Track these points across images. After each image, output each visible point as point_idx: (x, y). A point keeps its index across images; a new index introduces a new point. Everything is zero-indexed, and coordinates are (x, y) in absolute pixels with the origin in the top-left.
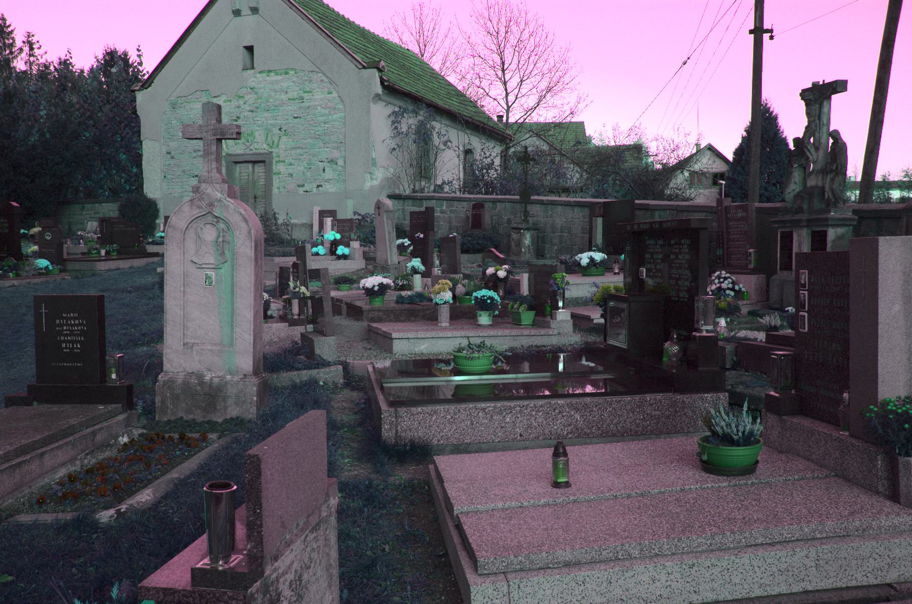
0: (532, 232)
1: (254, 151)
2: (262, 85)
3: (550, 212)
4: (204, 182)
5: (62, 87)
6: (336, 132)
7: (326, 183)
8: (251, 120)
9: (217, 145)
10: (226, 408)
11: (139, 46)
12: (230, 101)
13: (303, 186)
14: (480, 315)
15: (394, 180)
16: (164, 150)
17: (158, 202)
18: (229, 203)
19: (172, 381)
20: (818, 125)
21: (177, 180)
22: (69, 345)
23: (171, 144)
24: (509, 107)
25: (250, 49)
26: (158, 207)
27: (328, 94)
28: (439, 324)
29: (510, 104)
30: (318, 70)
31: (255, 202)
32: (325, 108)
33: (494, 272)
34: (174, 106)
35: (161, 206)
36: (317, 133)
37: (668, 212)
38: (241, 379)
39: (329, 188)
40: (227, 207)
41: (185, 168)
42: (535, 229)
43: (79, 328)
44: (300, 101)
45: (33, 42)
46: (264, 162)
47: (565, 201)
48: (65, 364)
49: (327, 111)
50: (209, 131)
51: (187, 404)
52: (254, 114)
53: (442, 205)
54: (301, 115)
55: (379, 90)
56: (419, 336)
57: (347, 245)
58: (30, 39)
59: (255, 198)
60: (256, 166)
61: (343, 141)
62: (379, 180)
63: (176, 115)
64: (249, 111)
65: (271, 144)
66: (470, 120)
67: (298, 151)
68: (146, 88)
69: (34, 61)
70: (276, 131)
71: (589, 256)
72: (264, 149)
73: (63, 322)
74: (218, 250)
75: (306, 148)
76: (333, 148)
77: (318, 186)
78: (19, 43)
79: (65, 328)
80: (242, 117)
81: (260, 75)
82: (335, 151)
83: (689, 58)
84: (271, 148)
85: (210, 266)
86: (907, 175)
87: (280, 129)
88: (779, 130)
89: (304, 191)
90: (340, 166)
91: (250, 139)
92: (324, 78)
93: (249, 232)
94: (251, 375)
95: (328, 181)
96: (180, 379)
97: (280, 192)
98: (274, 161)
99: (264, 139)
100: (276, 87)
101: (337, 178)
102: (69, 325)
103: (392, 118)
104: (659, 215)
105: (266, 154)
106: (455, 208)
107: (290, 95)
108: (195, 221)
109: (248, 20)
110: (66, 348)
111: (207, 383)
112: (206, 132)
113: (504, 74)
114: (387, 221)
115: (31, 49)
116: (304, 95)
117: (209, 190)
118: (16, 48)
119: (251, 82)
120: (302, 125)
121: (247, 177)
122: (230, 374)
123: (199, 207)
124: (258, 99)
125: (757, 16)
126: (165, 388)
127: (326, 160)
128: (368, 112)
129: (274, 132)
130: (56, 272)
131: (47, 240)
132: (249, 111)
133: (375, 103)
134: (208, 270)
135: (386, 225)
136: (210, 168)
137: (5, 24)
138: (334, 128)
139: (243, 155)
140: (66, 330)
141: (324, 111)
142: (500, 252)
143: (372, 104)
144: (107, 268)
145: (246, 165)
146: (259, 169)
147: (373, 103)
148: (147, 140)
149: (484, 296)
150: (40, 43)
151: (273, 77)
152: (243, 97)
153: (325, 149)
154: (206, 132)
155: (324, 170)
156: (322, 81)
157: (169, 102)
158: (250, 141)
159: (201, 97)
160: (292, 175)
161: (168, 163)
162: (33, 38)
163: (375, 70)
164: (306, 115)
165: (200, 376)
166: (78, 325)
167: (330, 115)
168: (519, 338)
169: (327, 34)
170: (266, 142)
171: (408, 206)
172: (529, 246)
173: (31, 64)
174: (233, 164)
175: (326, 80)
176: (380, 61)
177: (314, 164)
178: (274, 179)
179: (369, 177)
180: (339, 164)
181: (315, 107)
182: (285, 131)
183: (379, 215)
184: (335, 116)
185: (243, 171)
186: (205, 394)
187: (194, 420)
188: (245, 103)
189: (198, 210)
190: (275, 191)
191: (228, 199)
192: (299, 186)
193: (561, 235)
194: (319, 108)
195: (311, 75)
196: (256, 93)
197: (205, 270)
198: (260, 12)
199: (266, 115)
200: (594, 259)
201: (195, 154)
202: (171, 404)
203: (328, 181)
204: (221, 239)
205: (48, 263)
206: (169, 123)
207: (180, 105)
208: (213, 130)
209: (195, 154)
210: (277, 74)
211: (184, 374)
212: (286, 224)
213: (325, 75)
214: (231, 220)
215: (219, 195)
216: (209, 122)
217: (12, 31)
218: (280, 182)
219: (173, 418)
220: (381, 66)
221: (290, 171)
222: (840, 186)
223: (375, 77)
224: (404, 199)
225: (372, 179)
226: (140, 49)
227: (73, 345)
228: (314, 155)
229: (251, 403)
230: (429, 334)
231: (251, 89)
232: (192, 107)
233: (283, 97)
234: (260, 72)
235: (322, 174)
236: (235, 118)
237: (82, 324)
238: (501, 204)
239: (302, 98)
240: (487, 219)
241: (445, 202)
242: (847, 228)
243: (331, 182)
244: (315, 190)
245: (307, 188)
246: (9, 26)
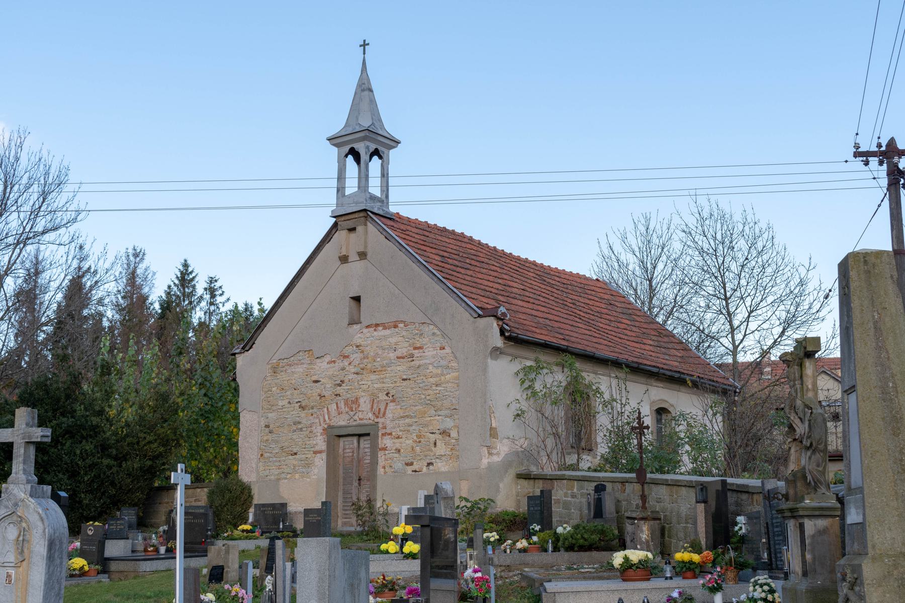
0: (652, 522)
1: (359, 422)
2: (369, 342)
3: (675, 496)
4: (12, 483)
5: (179, 350)
7: (438, 460)
8: (356, 384)
9: (25, 448)
11: (261, 299)
12: (334, 362)
13: (411, 464)
16: (263, 424)
17: (252, 487)
20: (799, 390)
21: (275, 459)
23: (270, 415)
25: (357, 299)
26: (252, 494)
30: (429, 322)
31: (360, 485)
32: (437, 367)
34: (275, 370)
35: (255, 491)
36: (428, 398)
39: (441, 466)
40: (27, 507)
41: (283, 445)
42: (654, 519)
44: (410, 359)
45: (215, 288)
46: (368, 435)
49: (439, 371)
50: (19, 435)
52: (359, 377)
53: (573, 487)
54: (410, 377)
55: (499, 342)
58: (213, 285)
59: (360, 480)
60: (362, 439)
62: (503, 455)
63: (276, 381)
64: (354, 373)
65: (377, 413)
67: (408, 421)
68: (248, 351)
69: (214, 311)
70: (382, 397)
72: (370, 419)
74: (18, 548)
75: (415, 416)
76: (446, 416)
77: (429, 464)
78: (200, 290)
80: (346, 379)
81: (367, 330)
82: (448, 419)
84: (377, 417)
85: (11, 565)
87: (387, 394)
89: (413, 471)
90: (453, 438)
91: (354, 406)
93: (44, 531)
95: (440, 457)
97: (385, 473)
98: (380, 434)
99: (369, 406)
100: (384, 343)
105: (372, 425)
107: (399, 353)
108: (6, 518)
109: (356, 267)
112: (17, 436)
113: (727, 304)
114: (445, 510)
115: (213, 296)
116: (414, 351)
117: (16, 491)
118: (196, 297)
119: (358, 339)
120: (412, 388)
121: (351, 454)
123: (6, 507)
124: (364, 358)
125: (894, 237)
127: (437, 432)
128: (485, 370)
129: (381, 398)
130: (93, 573)
131: (88, 535)
132: (354, 373)
133: (496, 358)
137: (187, 270)
138: (447, 391)
139: (345, 427)
141: (435, 371)
143: (489, 360)
144: (154, 569)
145: (349, 439)
146: (365, 443)
147: (491, 359)
148: (245, 411)
150: (223, 290)
151: (381, 332)
152: (347, 357)
154: (17, 436)
155: (435, 444)
156: (434, 334)
157: (270, 366)
158: (354, 409)
159: (303, 359)
160: (399, 451)
161: (265, 438)
162: (215, 284)
163: (492, 318)
164: (415, 376)
167: (442, 375)
169: (438, 278)
170: (372, 410)
172: (647, 541)
173: (211, 314)
174: (337, 438)
175: (438, 333)
176: (499, 307)
177: (424, 436)
178: (379, 456)
179: (486, 452)
180: (452, 436)
181: (426, 366)
182: (393, 396)
185: (347, 447)
188: (350, 364)
190: (380, 471)
192: (407, 464)
193: (685, 527)
194: (431, 367)
195: (422, 327)
196: (362, 352)
197: (7, 568)
198: (368, 257)
199: (373, 377)
200: (628, 558)
201: (294, 428)
203: (440, 457)
204: (21, 538)
205: (85, 562)
206: (268, 391)
207: (282, 369)
208: (23, 434)
209: (294, 428)
210: (385, 328)
212: (385, 514)
214: (30, 519)
217: (194, 278)
218: (386, 460)
220: (499, 313)
221: (398, 446)
222: (818, 466)
223: (492, 327)
224: (535, 479)
225: (490, 454)
226: (262, 302)
228: (426, 425)
231: (357, 346)
232: (293, 370)
233: (392, 355)
234: (367, 327)
235: (433, 449)
236: (338, 382)
238: (630, 484)
239: (412, 356)
240: (609, 506)
241: (576, 483)
242: (830, 520)
243: (443, 458)
244: (425, 469)
245: (416, 467)
246: (191, 273)
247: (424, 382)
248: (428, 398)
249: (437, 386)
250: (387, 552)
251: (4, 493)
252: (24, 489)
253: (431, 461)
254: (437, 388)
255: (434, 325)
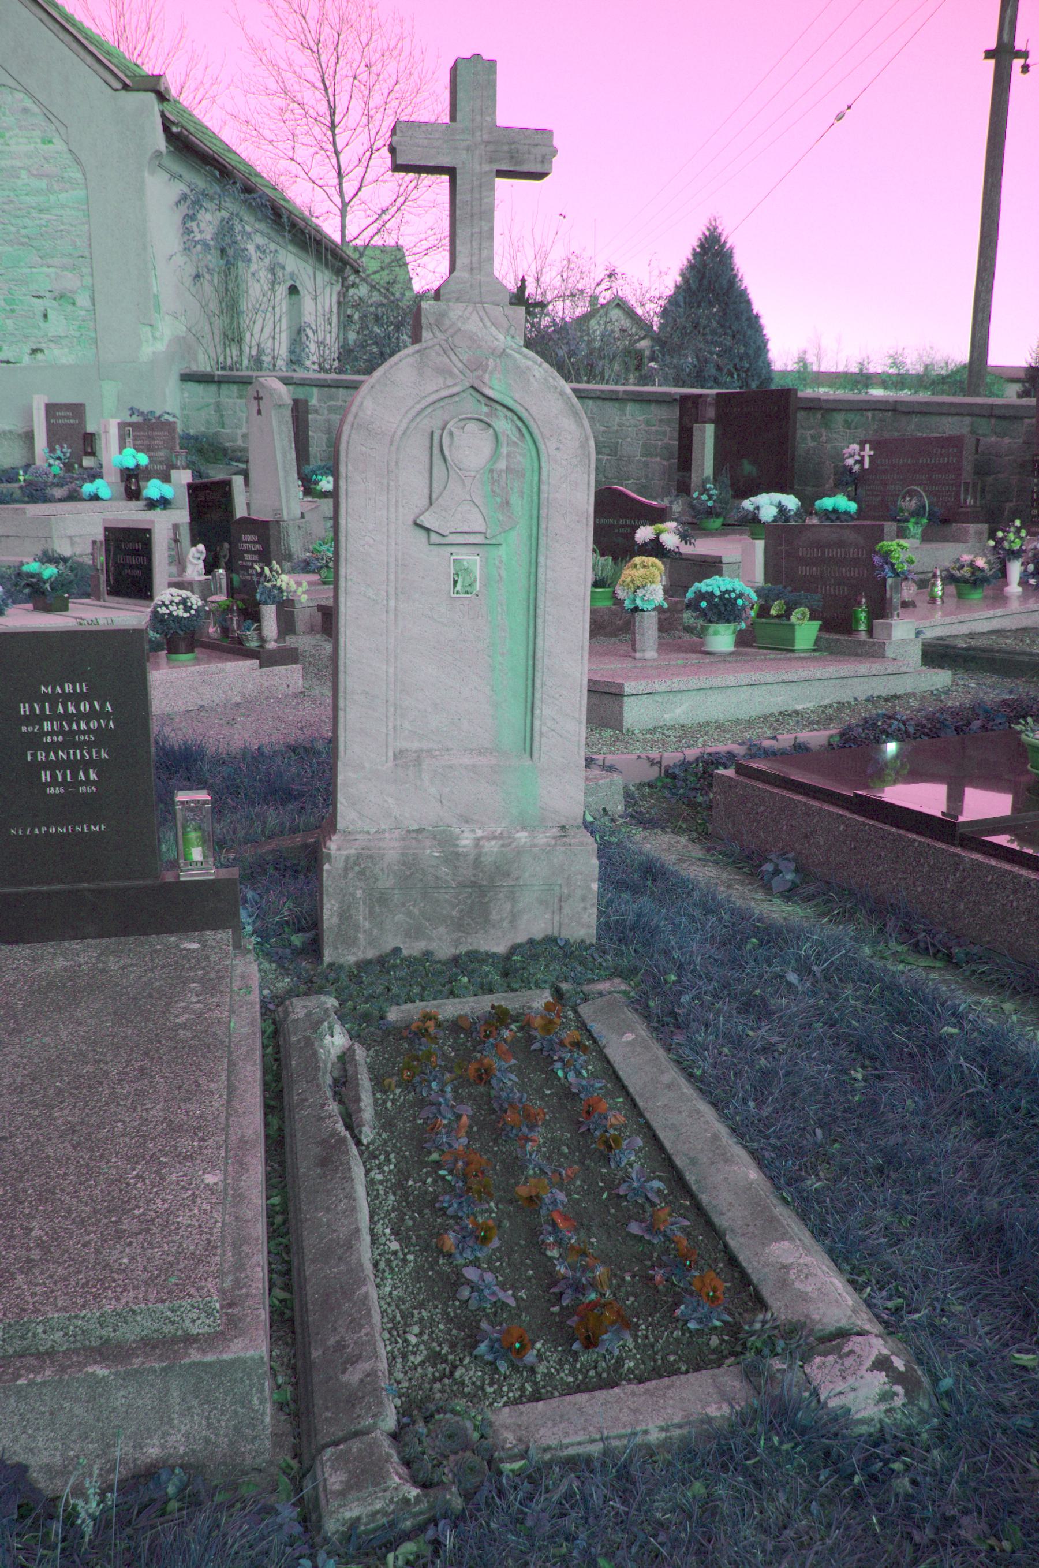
4: (458, 300)
6: (68, 232)
7: (52, 345)
10: (514, 917)
14: (716, 633)
15: (183, 346)
18: (530, 363)
19: (371, 857)
22: (64, 776)
24: (345, 205)
27: (44, 142)
28: (638, 655)
29: (347, 199)
32: (39, 176)
33: (653, 537)
36: (23, 231)
37: (870, 414)
38: (555, 838)
39: (59, 355)
43: (94, 724)
47: (602, 391)
48: (53, 830)
51: (409, 914)
55: (160, 142)
56: (676, 687)
57: (166, 479)
61: (87, 254)
66: (302, 224)
71: (776, 502)
73: (42, 709)
76: (64, 268)
77: (34, 351)
79: (47, 726)
82: (69, 275)
83: (849, 107)
86: (895, 364)
88: (736, 276)
92: (29, 103)
94: (578, 827)
95: (56, 340)
96: (391, 850)
101: (77, 334)
102: (60, 718)
103: (184, 209)
104: (846, 421)
106: (339, 403)
110: (54, 782)
111: (466, 855)
122: (524, 828)
123: (444, 371)
126: (351, 875)
127: (48, 294)
133: (152, 173)
134: (464, 549)
135: (276, 437)
136: (475, 259)
140: (52, 733)
142: (655, 499)
149: (728, 592)
153: (45, 269)
155: (45, 316)
156: (25, 110)
163: (152, 95)
165: (445, 840)
166: (87, 717)
168: (850, 681)
171: (229, 397)
175: (35, 108)
183: (259, 412)
184: (63, 196)
186: (462, 885)
187: (427, 954)
189: (441, 380)
191: (525, 350)
194: (24, 174)
197: (453, 549)
202: (365, 919)
203: (56, 340)
211: (397, 834)
213: (32, 96)
214: (534, 410)
215: (501, 339)
216: (478, 118)
219: (370, 954)
227: (75, 775)
229: (584, 899)
230: (694, 682)
235: (42, 324)
237: (101, 715)
241: (315, 390)
243: (64, 342)
244: (26, 359)
247: (12, 201)
248: (23, 231)
249: (41, 211)
250: (96, 498)
251: (430, 327)
252: (504, 321)
253: (38, 346)
254: (42, 216)
255: (27, 92)
